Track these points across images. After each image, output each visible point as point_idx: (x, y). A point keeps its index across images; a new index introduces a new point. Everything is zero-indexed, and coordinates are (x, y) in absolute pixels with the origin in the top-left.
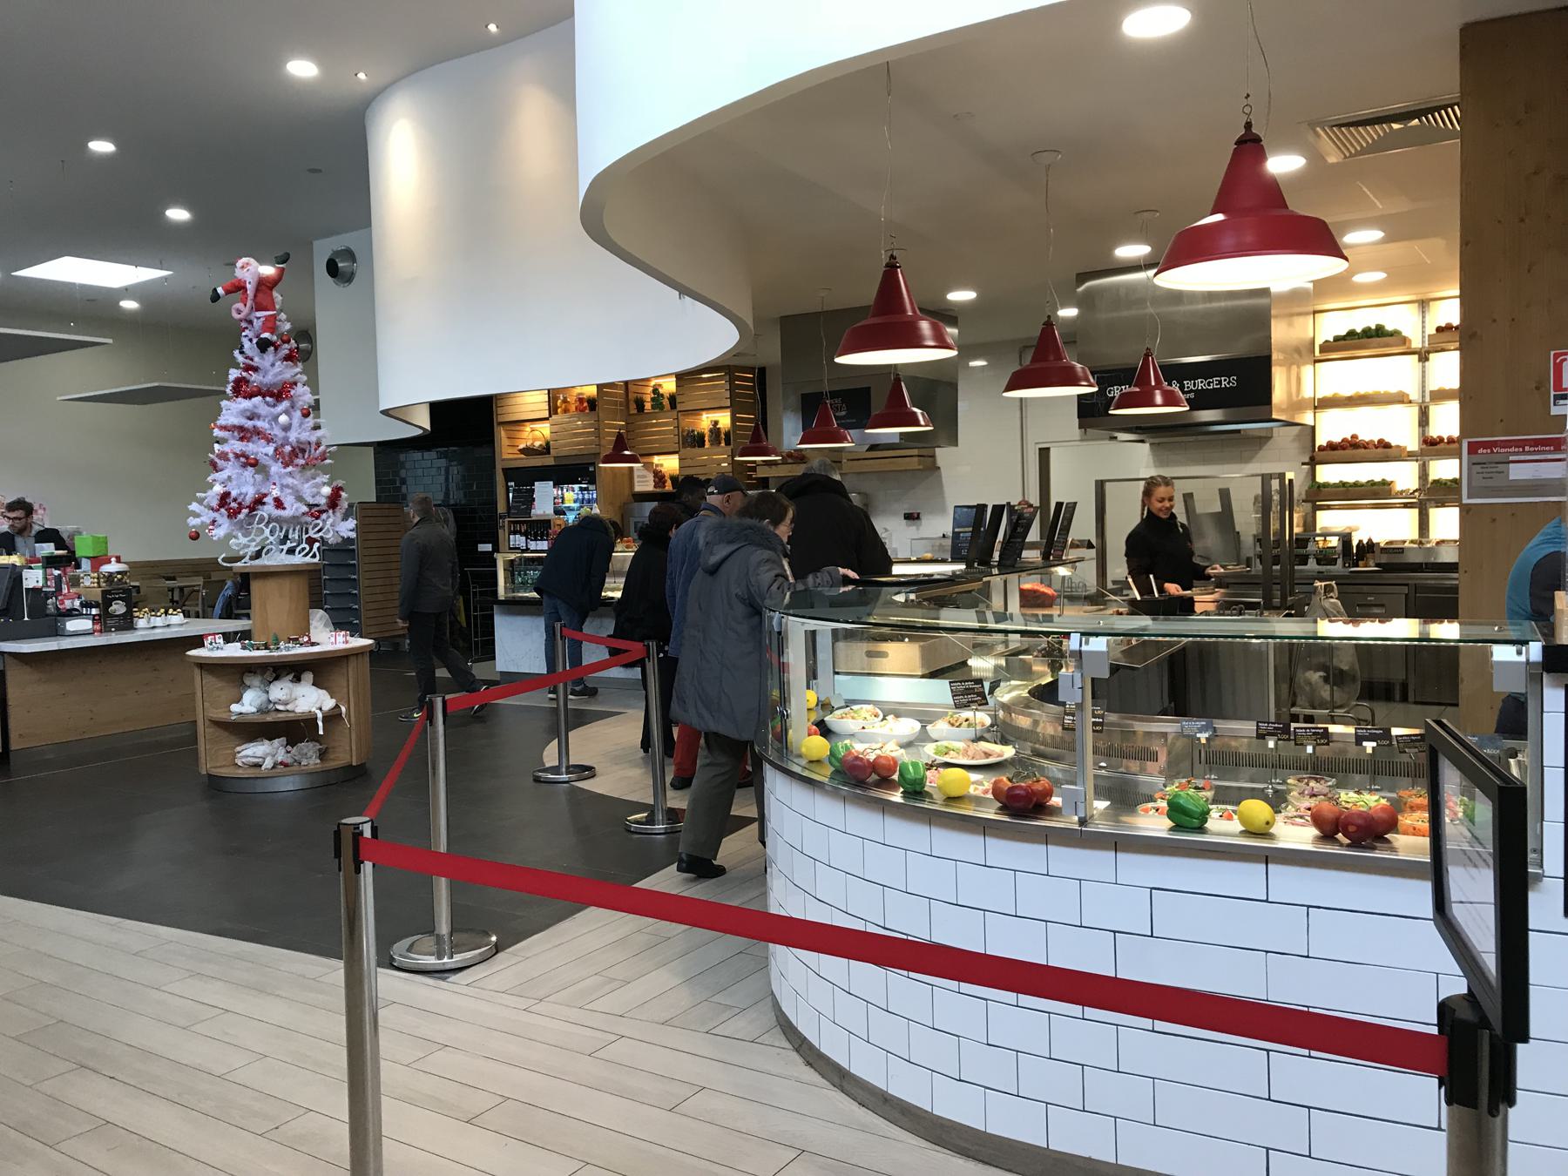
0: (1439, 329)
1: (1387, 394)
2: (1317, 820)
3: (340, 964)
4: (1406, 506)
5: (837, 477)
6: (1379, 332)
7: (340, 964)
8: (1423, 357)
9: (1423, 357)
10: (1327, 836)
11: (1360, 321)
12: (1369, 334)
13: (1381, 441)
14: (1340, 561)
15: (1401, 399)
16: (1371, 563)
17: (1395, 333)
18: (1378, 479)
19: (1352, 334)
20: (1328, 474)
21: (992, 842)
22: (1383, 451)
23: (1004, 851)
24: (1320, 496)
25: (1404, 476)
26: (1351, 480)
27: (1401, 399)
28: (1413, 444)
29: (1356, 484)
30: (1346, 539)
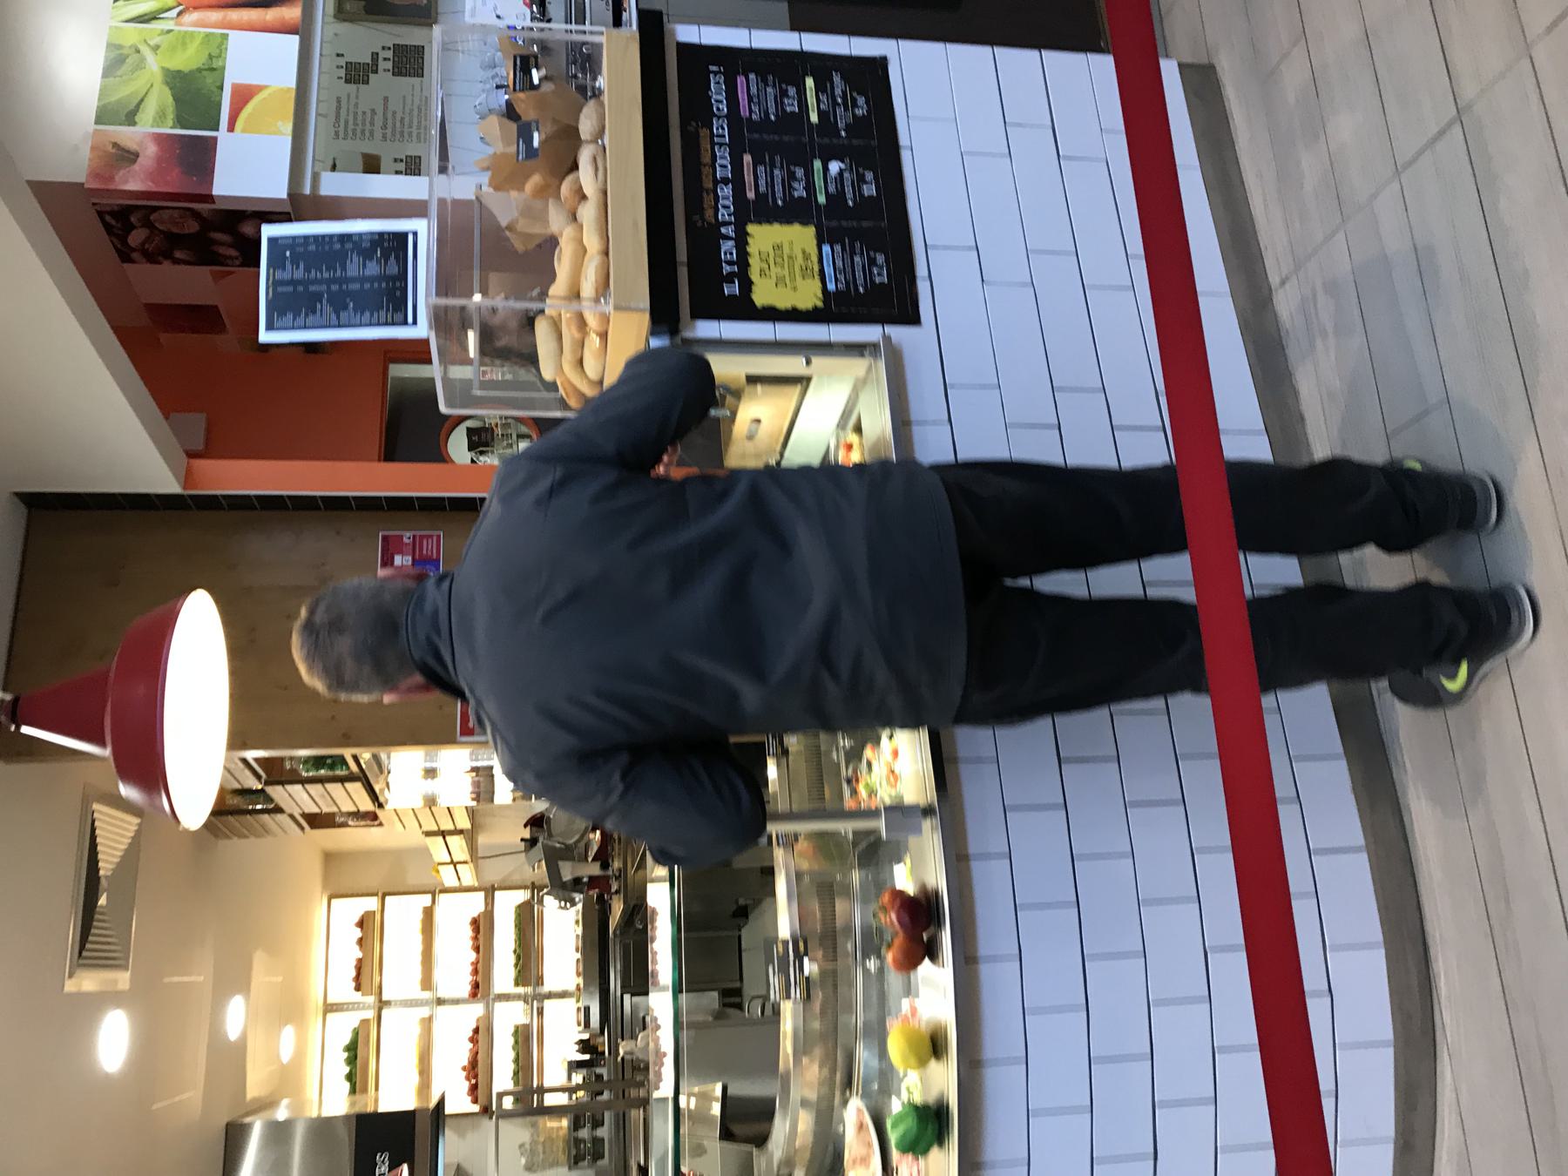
0: (358, 988)
1: (421, 1036)
2: (910, 962)
3: (1104, 65)
4: (541, 1012)
5: (665, 458)
6: (352, 1049)
7: (1104, 65)
8: (382, 1004)
9: (382, 1004)
10: (931, 951)
11: (338, 1067)
12: (352, 1060)
13: (472, 1040)
14: (599, 1070)
15: (428, 1023)
16: (600, 1040)
17: (356, 1033)
18: (512, 1040)
19: (350, 1077)
20: (503, 1078)
21: (984, 949)
22: (481, 1035)
23: (993, 934)
24: (529, 1102)
25: (509, 1016)
26: (512, 1067)
27: (428, 1023)
28: (477, 1009)
29: (516, 1061)
30: (574, 1066)
